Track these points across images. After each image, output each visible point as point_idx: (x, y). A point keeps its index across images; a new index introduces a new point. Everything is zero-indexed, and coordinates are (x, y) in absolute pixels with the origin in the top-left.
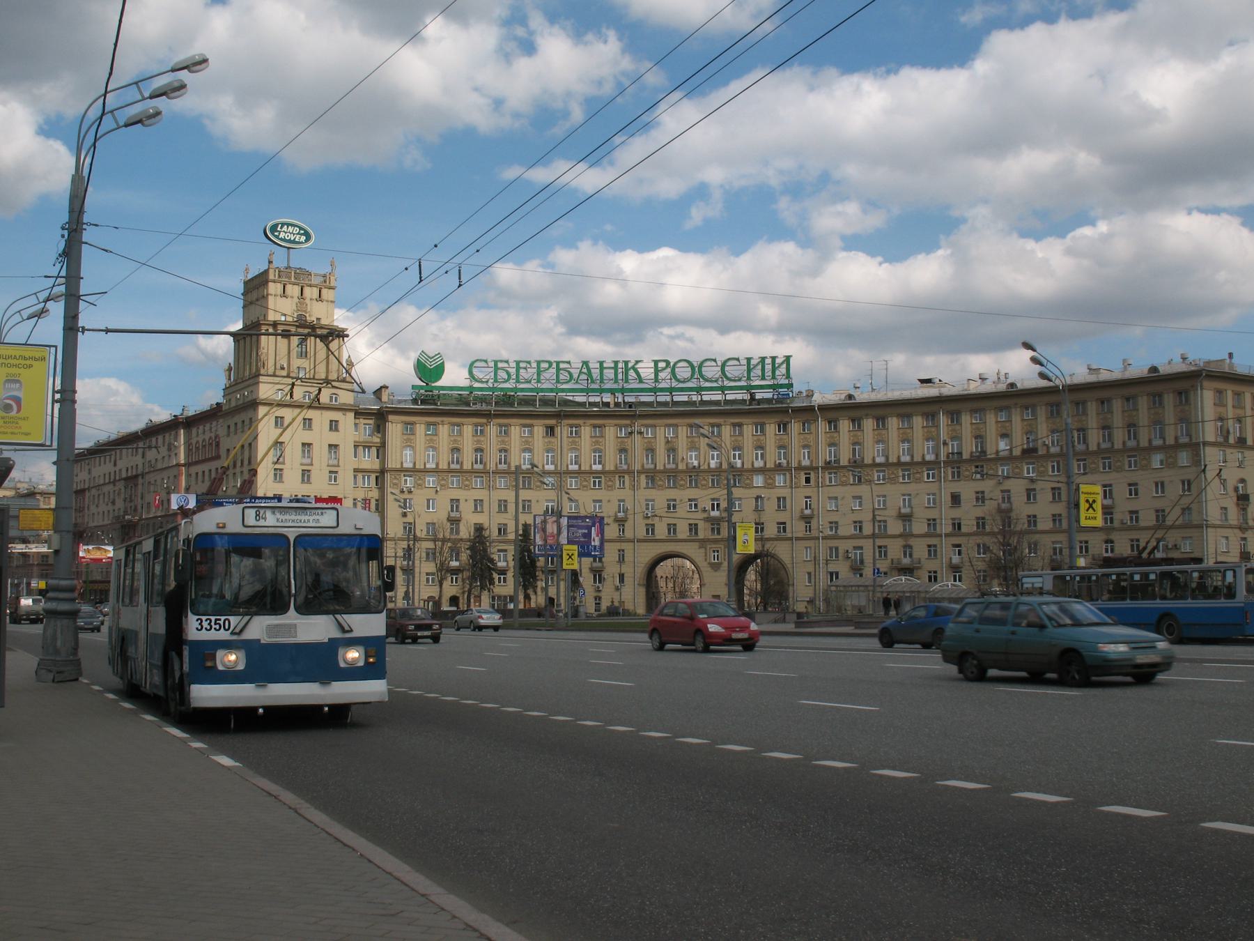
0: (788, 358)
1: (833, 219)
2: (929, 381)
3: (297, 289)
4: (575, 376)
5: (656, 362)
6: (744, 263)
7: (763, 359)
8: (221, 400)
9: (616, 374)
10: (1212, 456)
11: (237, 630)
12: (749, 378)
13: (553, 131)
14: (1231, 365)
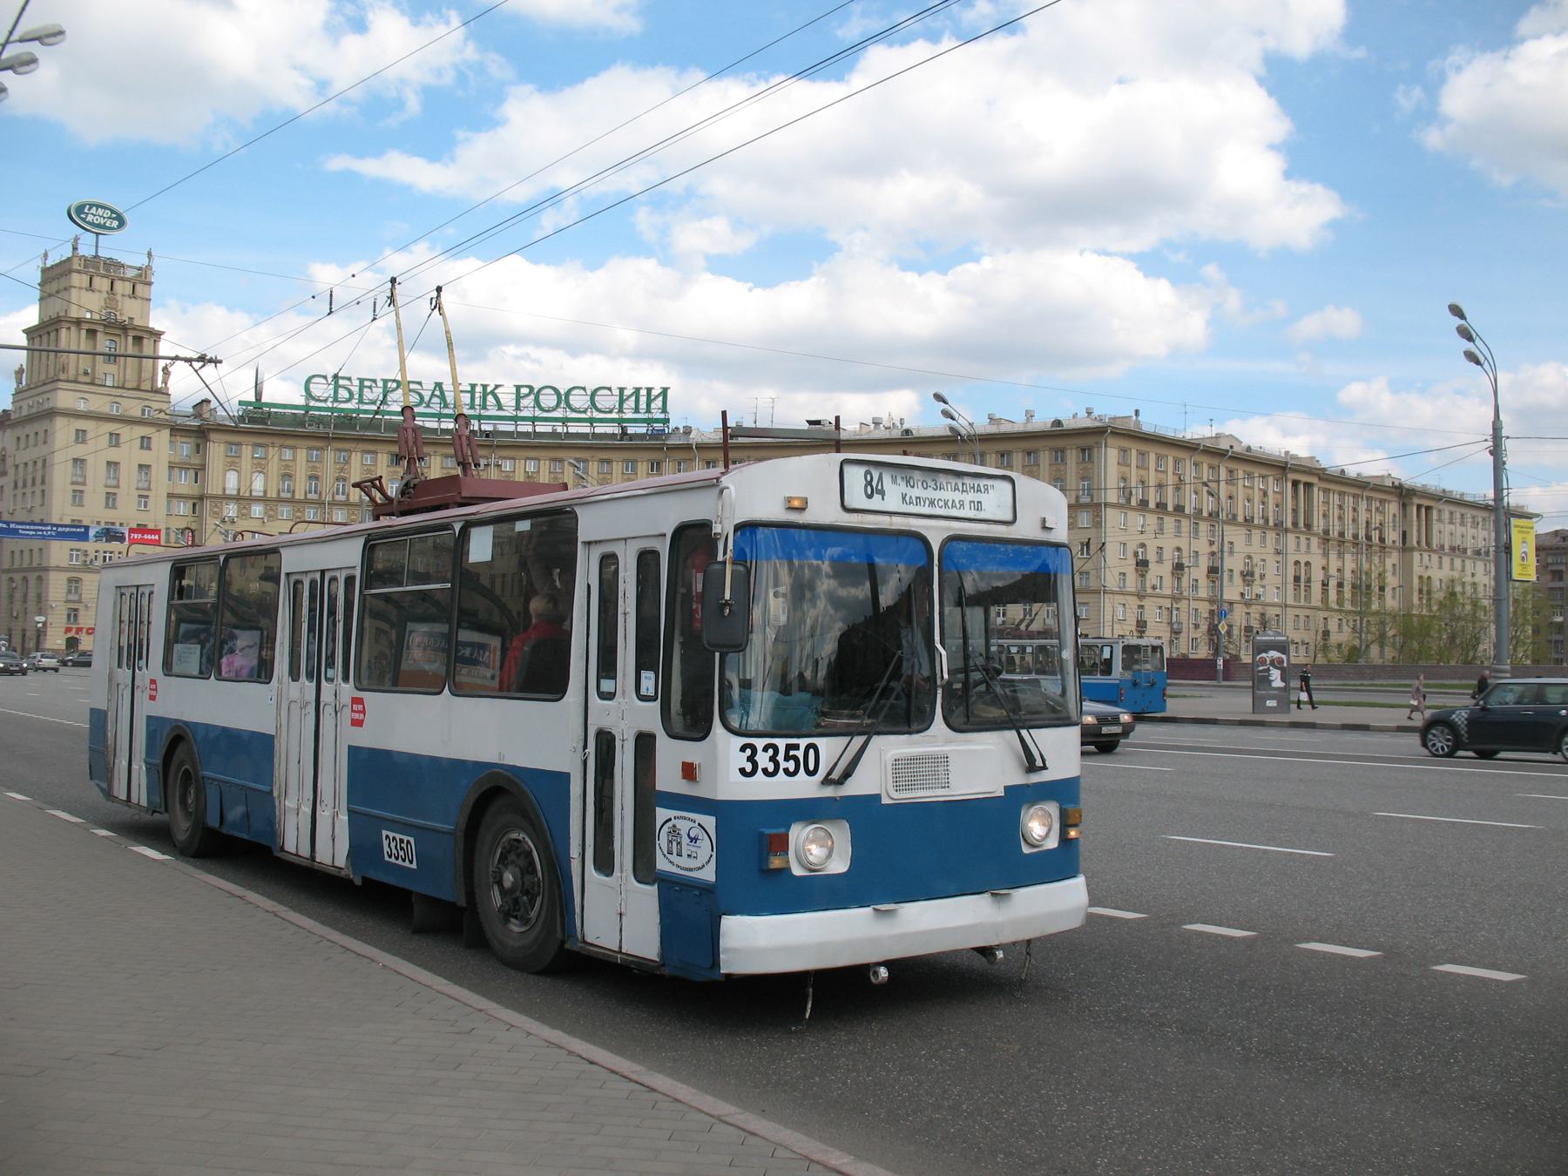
0: (665, 391)
1: (694, 236)
2: (818, 422)
3: (106, 284)
4: (427, 399)
5: (518, 388)
6: (598, 280)
7: (637, 390)
8: (9, 407)
9: (473, 398)
10: (1112, 517)
11: (835, 776)
12: (621, 411)
13: (375, 118)
14: (1137, 423)
